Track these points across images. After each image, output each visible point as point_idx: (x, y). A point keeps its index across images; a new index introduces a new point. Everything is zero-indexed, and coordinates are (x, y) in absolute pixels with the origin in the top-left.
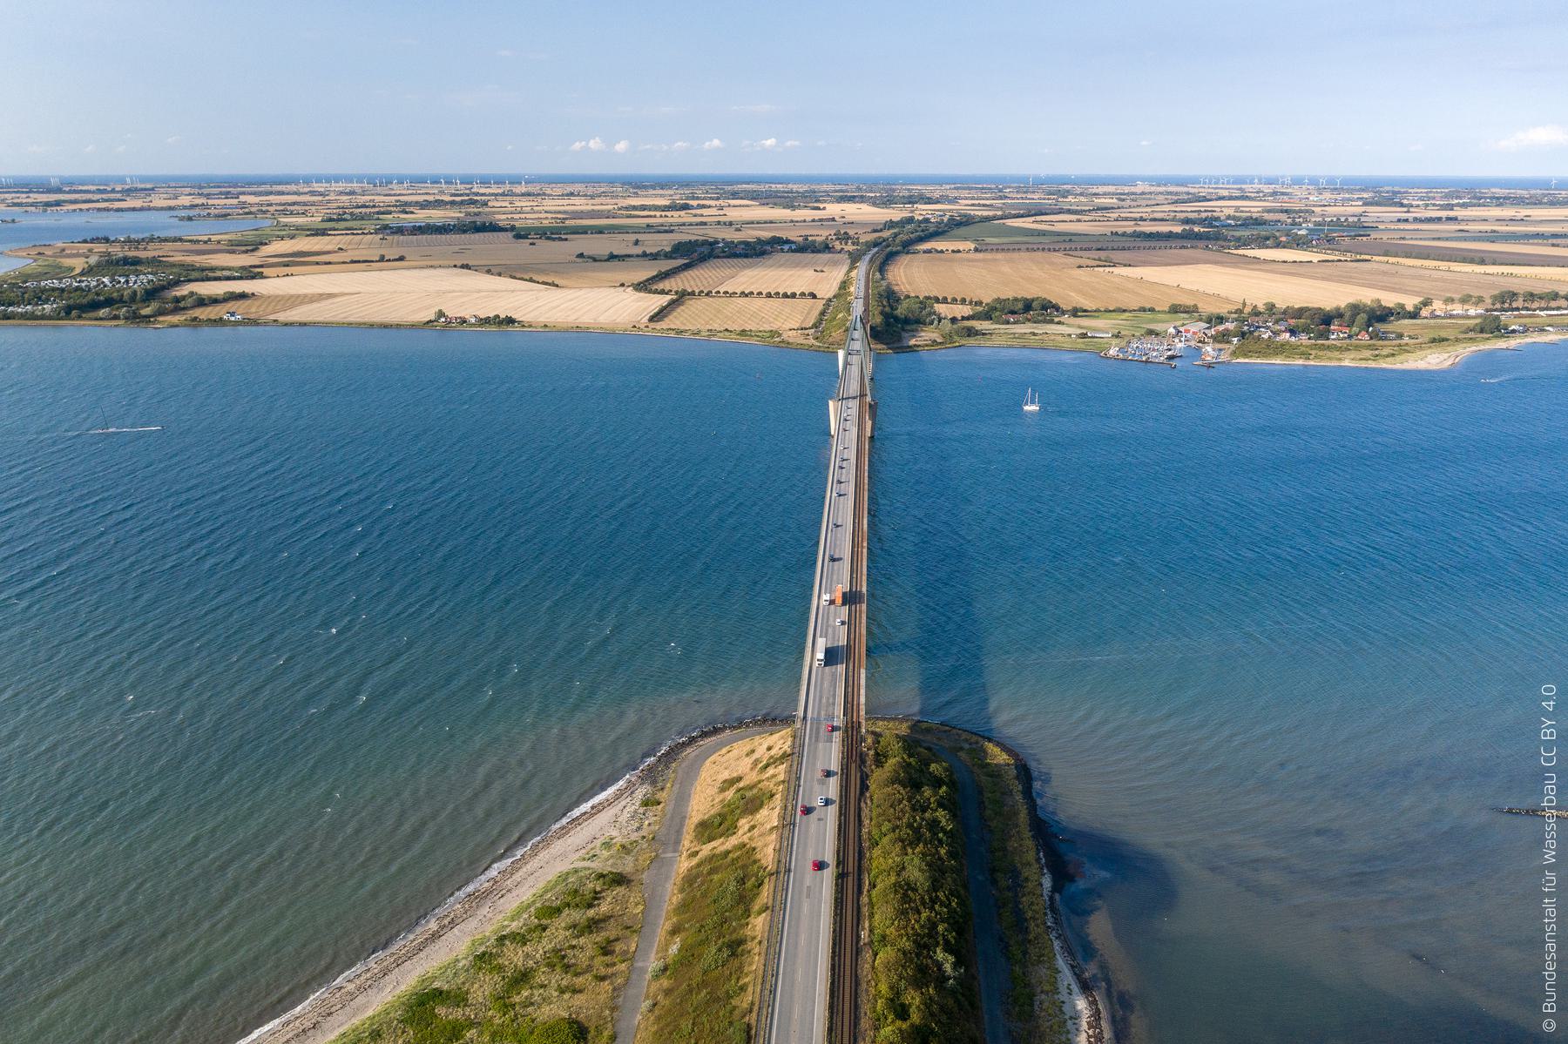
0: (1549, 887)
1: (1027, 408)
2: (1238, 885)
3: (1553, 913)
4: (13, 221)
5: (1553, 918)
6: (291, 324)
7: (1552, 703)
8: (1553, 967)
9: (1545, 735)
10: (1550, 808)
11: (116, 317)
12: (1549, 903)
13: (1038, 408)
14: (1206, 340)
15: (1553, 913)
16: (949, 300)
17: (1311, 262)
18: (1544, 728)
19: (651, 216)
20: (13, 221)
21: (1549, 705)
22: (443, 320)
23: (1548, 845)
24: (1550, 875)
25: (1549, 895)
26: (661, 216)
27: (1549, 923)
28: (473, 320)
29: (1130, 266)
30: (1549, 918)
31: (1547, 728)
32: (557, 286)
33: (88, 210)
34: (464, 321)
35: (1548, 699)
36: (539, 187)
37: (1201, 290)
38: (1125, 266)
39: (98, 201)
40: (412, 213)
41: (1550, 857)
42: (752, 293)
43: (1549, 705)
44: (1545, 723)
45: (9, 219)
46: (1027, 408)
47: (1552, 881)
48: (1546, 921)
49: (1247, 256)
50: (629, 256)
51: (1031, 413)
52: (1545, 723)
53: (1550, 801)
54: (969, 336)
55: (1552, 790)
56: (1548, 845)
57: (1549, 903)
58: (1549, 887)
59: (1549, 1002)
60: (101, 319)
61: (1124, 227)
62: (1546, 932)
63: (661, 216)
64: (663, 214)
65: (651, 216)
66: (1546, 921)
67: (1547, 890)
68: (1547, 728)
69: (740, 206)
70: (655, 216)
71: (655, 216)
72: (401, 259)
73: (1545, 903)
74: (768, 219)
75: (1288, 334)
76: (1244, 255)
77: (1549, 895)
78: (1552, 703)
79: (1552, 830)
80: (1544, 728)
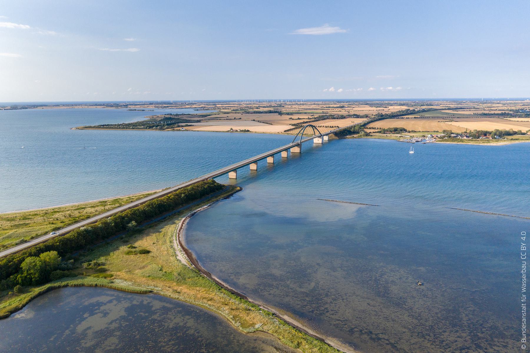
0: (524, 300)
1: (410, 152)
2: (258, 278)
3: (525, 309)
4: (153, 110)
5: (525, 310)
6: (195, 131)
7: (524, 238)
8: (523, 267)
9: (522, 248)
10: (524, 273)
11: (157, 129)
12: (523, 305)
13: (413, 152)
14: (437, 138)
15: (525, 309)
16: (376, 128)
17: (528, 121)
18: (522, 246)
19: (328, 110)
20: (153, 110)
21: (524, 239)
22: (232, 130)
23: (525, 326)
24: (524, 296)
25: (524, 303)
26: (332, 109)
27: (524, 312)
28: (239, 131)
29: (457, 122)
30: (524, 310)
31: (523, 246)
32: (272, 124)
33: (174, 108)
34: (237, 131)
35: (523, 236)
36: (296, 102)
37: (464, 127)
38: (455, 122)
39: (178, 106)
40: (259, 109)
41: (524, 290)
42: (321, 126)
43: (524, 239)
44: (522, 244)
45: (152, 110)
46: (410, 152)
47: (525, 298)
48: (523, 311)
49: (511, 120)
50: (239, 119)
51: (412, 154)
52: (522, 244)
53: (524, 271)
54: (366, 136)
55: (525, 267)
56: (525, 326)
57: (523, 305)
58: (524, 300)
59: (524, 339)
60: (153, 129)
61: (487, 112)
62: (523, 315)
63: (332, 109)
64: (332, 109)
65: (328, 110)
66: (523, 311)
67: (523, 301)
68: (523, 246)
69: (362, 107)
70: (330, 110)
71: (330, 110)
72: (240, 119)
73: (522, 306)
74: (316, 113)
75: (465, 137)
76: (510, 120)
77: (524, 303)
78: (524, 238)
79: (525, 281)
80: (522, 246)
